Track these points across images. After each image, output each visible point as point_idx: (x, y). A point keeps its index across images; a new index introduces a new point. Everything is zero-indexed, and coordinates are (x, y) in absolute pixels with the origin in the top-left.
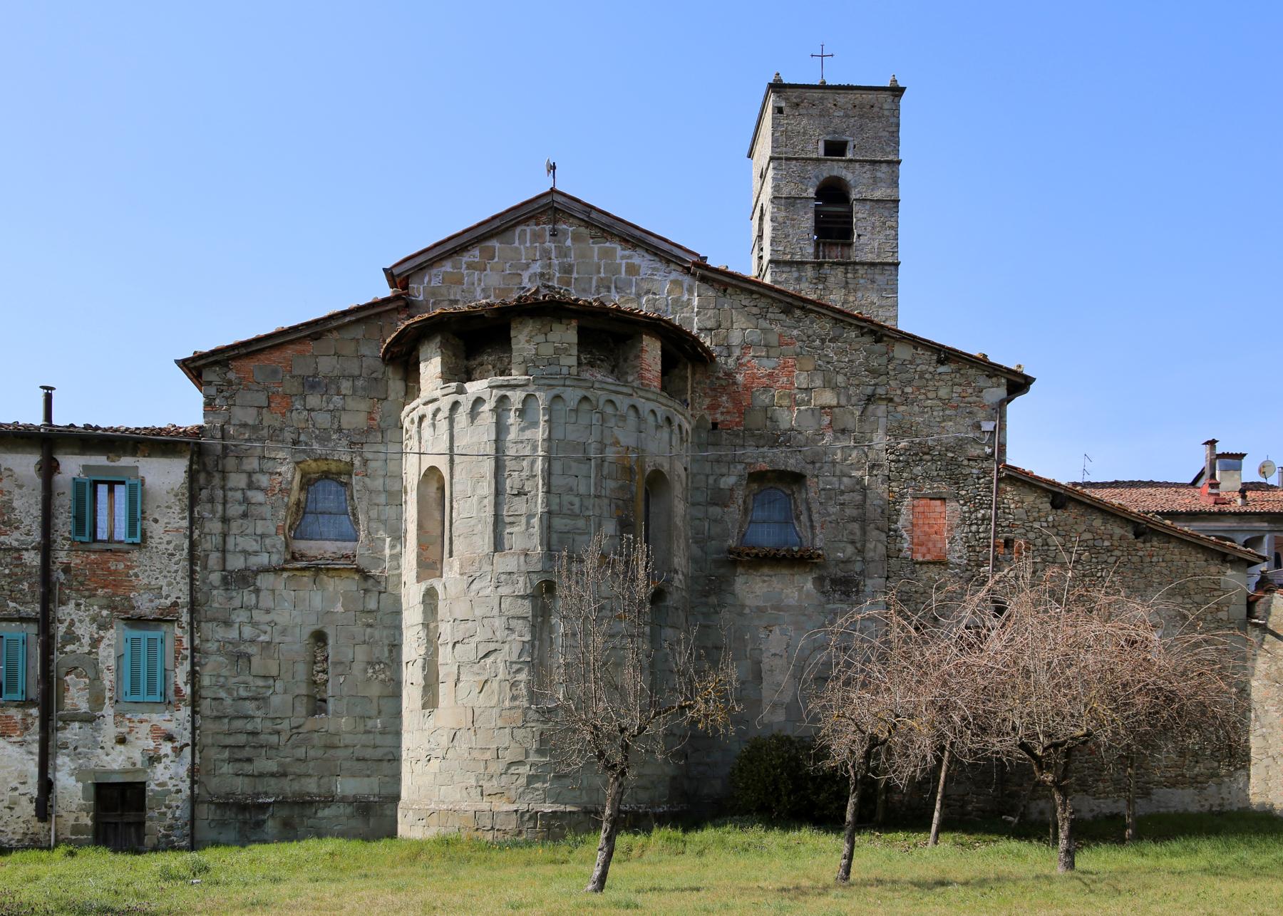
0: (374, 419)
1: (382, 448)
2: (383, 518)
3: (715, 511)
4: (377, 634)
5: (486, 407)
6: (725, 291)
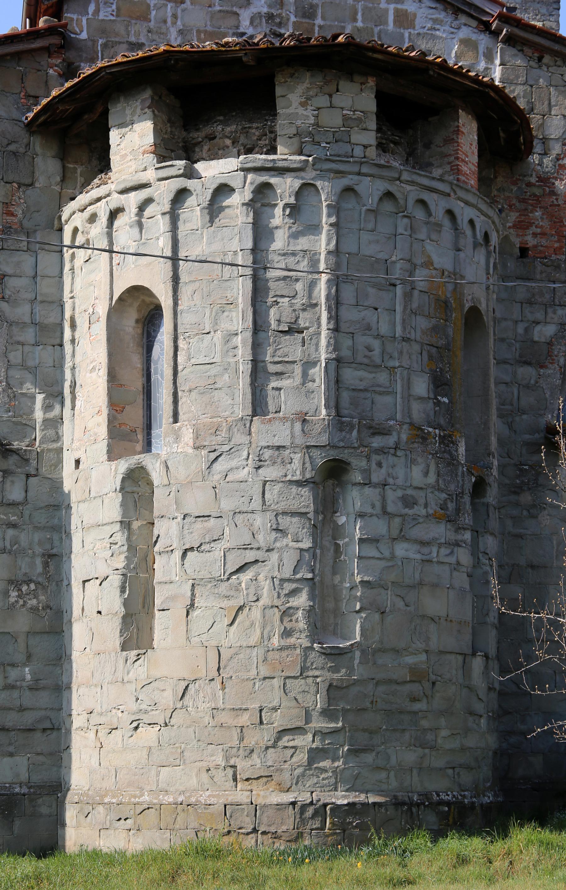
0: (12, 215)
1: (27, 260)
2: (30, 363)
3: (526, 373)
4: (23, 538)
5: (235, 200)
6: (540, 59)
